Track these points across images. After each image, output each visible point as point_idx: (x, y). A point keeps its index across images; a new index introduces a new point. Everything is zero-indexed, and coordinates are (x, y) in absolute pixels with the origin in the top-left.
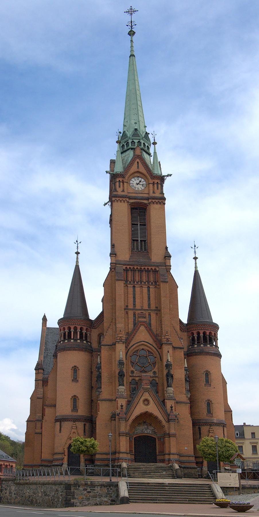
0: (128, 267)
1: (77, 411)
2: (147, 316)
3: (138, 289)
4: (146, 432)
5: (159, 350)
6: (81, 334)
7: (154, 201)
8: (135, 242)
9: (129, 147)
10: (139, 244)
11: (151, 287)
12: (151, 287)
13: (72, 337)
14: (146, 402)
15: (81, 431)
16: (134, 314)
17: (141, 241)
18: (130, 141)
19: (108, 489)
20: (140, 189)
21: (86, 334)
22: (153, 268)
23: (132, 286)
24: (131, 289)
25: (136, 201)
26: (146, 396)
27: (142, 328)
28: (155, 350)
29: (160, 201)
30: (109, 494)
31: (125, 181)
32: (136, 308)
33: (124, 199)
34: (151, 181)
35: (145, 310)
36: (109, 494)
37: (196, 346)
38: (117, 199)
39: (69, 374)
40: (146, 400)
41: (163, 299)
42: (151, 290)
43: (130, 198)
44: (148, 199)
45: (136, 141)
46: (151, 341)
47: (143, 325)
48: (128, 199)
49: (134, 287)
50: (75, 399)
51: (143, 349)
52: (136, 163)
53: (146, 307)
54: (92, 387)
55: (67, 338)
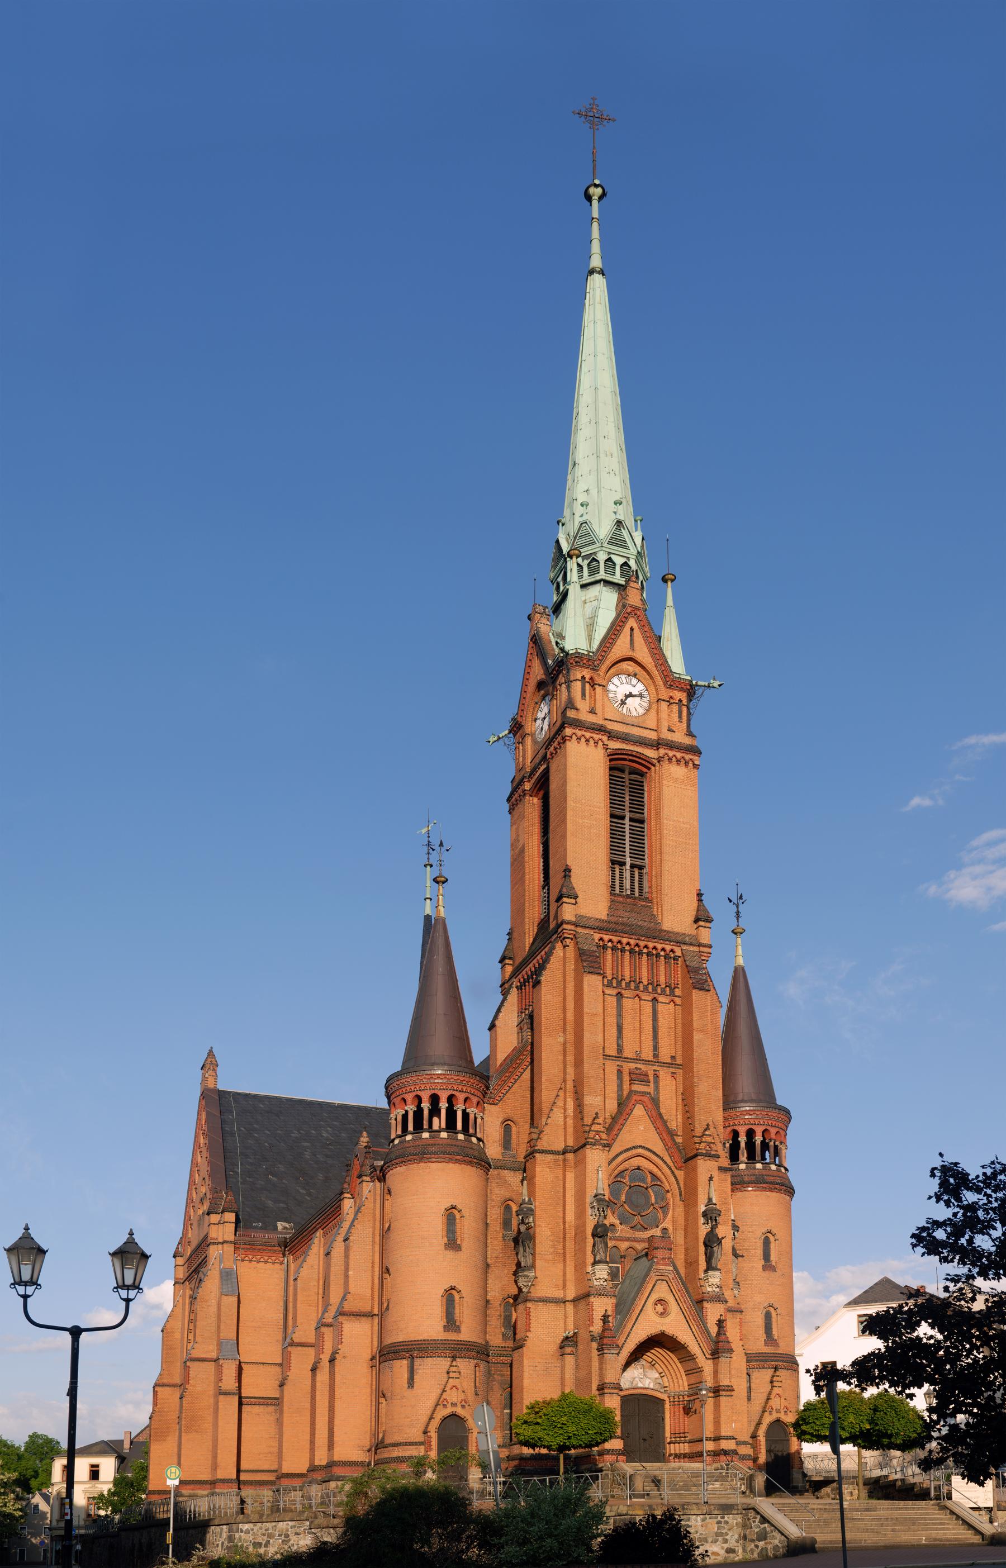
0: (606, 938)
1: (457, 1329)
2: (651, 1078)
3: (627, 1003)
4: (640, 1385)
5: (680, 1174)
6: (451, 1114)
7: (671, 753)
8: (617, 868)
9: (598, 577)
10: (627, 875)
11: (661, 999)
12: (661, 999)
13: (426, 1126)
14: (660, 1308)
15: (468, 1385)
16: (620, 1072)
17: (632, 866)
18: (602, 557)
19: (719, 1522)
20: (634, 714)
21: (466, 1115)
22: (668, 948)
23: (614, 992)
24: (612, 1001)
25: (624, 746)
26: (662, 1291)
27: (639, 1111)
28: (669, 1172)
29: (688, 757)
30: (722, 1534)
31: (598, 680)
32: (625, 1055)
33: (597, 737)
34: (665, 693)
35: (645, 1062)
36: (722, 1534)
37: (742, 1166)
38: (579, 733)
39: (437, 1226)
40: (660, 1301)
41: (697, 1037)
42: (661, 1007)
43: (612, 735)
44: (657, 745)
45: (619, 561)
46: (659, 1147)
47: (642, 1103)
48: (605, 738)
49: (619, 995)
50: (450, 1296)
51: (638, 1168)
52: (627, 630)
53: (648, 1054)
54: (488, 1266)
55: (411, 1128)
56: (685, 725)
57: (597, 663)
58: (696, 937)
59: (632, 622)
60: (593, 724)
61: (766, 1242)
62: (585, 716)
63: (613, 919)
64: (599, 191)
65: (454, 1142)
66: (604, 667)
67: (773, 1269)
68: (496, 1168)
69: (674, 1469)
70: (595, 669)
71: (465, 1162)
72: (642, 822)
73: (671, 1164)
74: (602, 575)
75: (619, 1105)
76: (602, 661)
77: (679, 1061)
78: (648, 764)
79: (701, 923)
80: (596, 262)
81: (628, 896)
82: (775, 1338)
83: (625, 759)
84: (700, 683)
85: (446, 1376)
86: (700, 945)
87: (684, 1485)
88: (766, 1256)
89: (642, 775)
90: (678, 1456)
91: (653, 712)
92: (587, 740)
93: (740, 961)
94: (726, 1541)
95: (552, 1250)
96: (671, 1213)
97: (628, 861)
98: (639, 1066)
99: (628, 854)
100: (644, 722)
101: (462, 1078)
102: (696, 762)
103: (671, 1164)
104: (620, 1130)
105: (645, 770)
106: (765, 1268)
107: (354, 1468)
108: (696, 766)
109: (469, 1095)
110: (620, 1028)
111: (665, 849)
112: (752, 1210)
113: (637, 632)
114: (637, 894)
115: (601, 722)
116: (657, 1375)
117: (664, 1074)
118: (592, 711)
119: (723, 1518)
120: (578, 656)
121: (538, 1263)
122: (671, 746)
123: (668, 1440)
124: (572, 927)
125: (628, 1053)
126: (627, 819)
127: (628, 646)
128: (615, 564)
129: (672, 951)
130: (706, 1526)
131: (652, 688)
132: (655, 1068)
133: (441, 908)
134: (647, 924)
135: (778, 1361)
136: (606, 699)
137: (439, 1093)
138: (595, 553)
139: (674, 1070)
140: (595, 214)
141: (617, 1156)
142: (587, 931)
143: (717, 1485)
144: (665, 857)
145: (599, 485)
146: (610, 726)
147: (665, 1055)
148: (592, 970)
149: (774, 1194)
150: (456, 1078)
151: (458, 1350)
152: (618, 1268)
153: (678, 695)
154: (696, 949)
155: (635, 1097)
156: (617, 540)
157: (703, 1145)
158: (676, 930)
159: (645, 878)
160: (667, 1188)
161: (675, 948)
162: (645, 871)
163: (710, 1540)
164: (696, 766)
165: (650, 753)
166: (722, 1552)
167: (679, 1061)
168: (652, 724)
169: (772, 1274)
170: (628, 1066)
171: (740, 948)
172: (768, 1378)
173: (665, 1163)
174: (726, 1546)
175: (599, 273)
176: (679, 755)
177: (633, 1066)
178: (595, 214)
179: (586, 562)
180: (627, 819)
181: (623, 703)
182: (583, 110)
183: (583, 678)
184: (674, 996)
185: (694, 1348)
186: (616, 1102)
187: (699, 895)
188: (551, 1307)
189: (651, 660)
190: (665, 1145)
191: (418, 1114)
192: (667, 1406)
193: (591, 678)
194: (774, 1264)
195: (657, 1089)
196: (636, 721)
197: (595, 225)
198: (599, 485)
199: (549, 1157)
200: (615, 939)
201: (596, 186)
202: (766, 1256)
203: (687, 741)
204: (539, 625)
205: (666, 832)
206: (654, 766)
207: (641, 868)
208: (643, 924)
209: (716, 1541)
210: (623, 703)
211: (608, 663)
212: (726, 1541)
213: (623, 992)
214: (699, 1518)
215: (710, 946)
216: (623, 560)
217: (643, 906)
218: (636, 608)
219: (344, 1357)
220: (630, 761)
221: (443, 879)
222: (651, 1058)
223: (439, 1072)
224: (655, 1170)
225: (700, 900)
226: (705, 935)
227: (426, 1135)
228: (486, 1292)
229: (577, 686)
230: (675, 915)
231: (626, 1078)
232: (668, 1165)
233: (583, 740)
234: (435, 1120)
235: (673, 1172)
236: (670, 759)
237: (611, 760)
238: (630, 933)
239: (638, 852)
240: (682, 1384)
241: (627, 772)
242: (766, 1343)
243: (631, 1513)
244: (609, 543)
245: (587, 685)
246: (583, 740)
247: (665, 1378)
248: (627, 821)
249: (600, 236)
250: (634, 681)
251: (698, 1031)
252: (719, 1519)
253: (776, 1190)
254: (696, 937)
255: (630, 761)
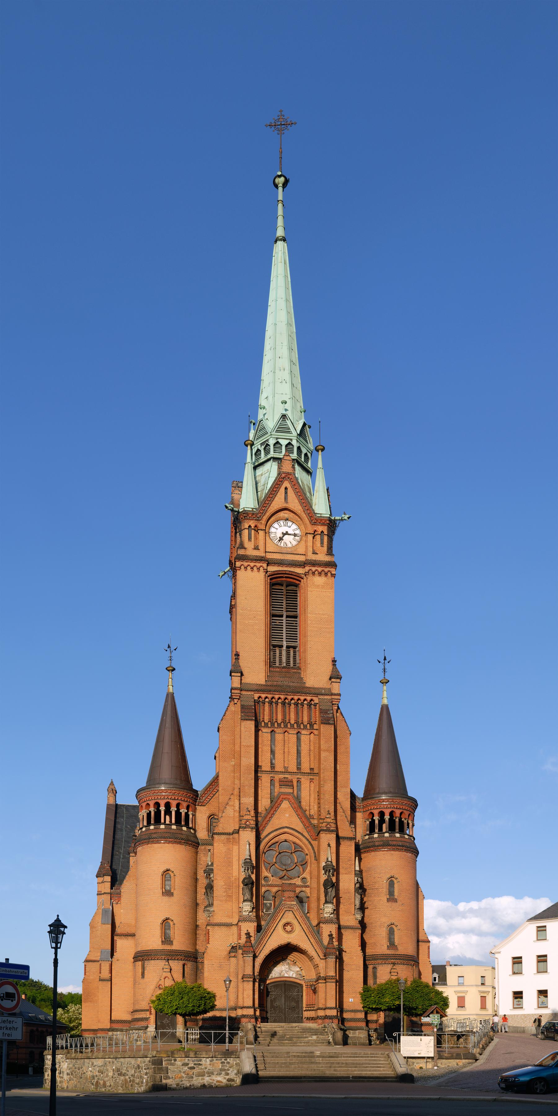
1: (171, 943)
4: (286, 975)
6: (178, 814)
7: (314, 569)
10: (284, 653)
13: (162, 821)
16: (272, 781)
17: (288, 647)
18: (272, 442)
19: (222, 1063)
20: (289, 545)
23: (269, 730)
28: (307, 842)
29: (326, 570)
30: (224, 1070)
32: (276, 770)
34: (311, 529)
36: (224, 1070)
38: (246, 564)
42: (303, 738)
46: (300, 827)
51: (286, 841)
52: (282, 490)
53: (293, 768)
55: (152, 822)
56: (325, 548)
57: (265, 513)
58: (330, 689)
59: (286, 484)
60: (257, 556)
61: (391, 884)
62: (251, 552)
63: (269, 683)
64: (282, 179)
65: (168, 831)
66: (265, 518)
67: (395, 901)
68: (203, 844)
69: (292, 1027)
70: (258, 520)
71: (175, 842)
72: (296, 617)
73: (309, 837)
74: (272, 454)
75: (272, 801)
76: (264, 513)
77: (316, 771)
78: (299, 577)
79: (333, 680)
80: (280, 232)
81: (284, 667)
82: (396, 944)
83: (282, 577)
84: (337, 518)
85: (162, 971)
86: (332, 694)
87: (289, 1038)
88: (391, 893)
89: (297, 586)
90: (308, 1019)
91: (303, 542)
92: (252, 568)
93: (385, 701)
94: (227, 1074)
95: (224, 894)
96: (309, 868)
97: (285, 644)
98: (286, 776)
99: (284, 640)
100: (295, 550)
101: (174, 792)
102: (333, 573)
103: (309, 837)
104: (271, 817)
105: (298, 582)
106: (388, 900)
107: (124, 1024)
108: (333, 575)
109: (180, 802)
110: (299, 752)
111: (309, 633)
112: (384, 863)
113: (290, 491)
114: (292, 665)
115: (263, 555)
116: (298, 969)
117: (305, 782)
118: (256, 548)
119: (226, 1060)
120: (245, 512)
121: (215, 903)
122: (314, 563)
123: (304, 1009)
124: (238, 691)
125: (279, 767)
126: (285, 616)
127: (283, 500)
128: (281, 446)
129: (312, 700)
130: (213, 1065)
131: (303, 526)
132: (298, 776)
133: (171, 687)
134: (299, 685)
135: (396, 959)
136: (267, 538)
137: (159, 801)
138: (267, 440)
139: (312, 777)
140: (280, 197)
141: (269, 834)
142: (249, 693)
143: (314, 1037)
144: (309, 639)
145: (279, 390)
146: (269, 556)
147: (305, 767)
148: (247, 718)
149: (397, 853)
150: (169, 791)
151: (171, 955)
152: (271, 904)
153: (320, 528)
154: (329, 697)
155: (282, 797)
156: (282, 428)
157: (324, 824)
158: (316, 686)
159: (297, 653)
160: (307, 852)
161: (314, 698)
162: (297, 649)
163: (215, 1073)
164: (333, 575)
165: (299, 571)
166: (225, 1081)
167: (316, 771)
168: (301, 550)
169: (394, 904)
170: (277, 777)
171: (385, 692)
172: (388, 970)
173: (304, 836)
174: (227, 1077)
175: (281, 240)
176: (320, 569)
177: (282, 776)
178: (280, 197)
179: (263, 447)
180: (285, 616)
181: (281, 539)
182: (273, 122)
183: (250, 526)
184: (300, 728)
185: (311, 952)
186: (269, 800)
187: (334, 661)
188: (224, 929)
189: (300, 507)
190: (304, 825)
191: (158, 813)
192: (304, 988)
193: (256, 526)
194: (396, 897)
195: (299, 789)
196: (289, 551)
197: (280, 205)
198: (279, 390)
199: (223, 837)
200: (270, 696)
201: (280, 176)
202: (391, 893)
203: (328, 559)
204: (233, 495)
205: (309, 622)
206: (303, 578)
207: (295, 648)
208: (291, 684)
209: (220, 1074)
210: (281, 539)
211: (268, 514)
212: (227, 1074)
213: (276, 729)
214: (208, 1060)
215: (339, 695)
216: (287, 442)
217: (294, 673)
218: (289, 474)
219: (118, 960)
220: (286, 577)
221: (171, 668)
222: (295, 771)
223: (163, 788)
224: (298, 841)
225: (334, 665)
226: (336, 688)
227: (162, 827)
228: (196, 920)
229: (246, 533)
230: (315, 675)
231: (277, 784)
232: (306, 838)
233: (249, 568)
234: (168, 817)
235: (310, 842)
236: (314, 573)
237: (271, 579)
238: (279, 692)
239: (293, 636)
240: (312, 975)
241: (285, 585)
242: (388, 948)
243: (158, 1055)
244: (277, 431)
245: (253, 531)
246: (249, 568)
247: (303, 971)
248: (284, 618)
249: (284, 212)
250: (290, 523)
251: (324, 751)
252: (223, 1060)
253: (398, 850)
254: (330, 689)
255: (286, 577)
